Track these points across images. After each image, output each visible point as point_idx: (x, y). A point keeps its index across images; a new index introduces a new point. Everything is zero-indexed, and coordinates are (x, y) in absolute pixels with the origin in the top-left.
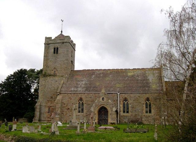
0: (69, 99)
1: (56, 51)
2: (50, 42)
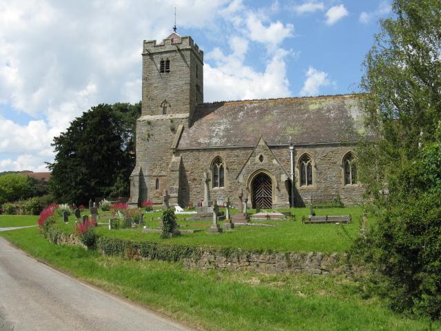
1: (165, 67)
2: (153, 50)
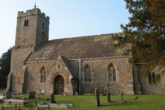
0: (33, 69)
1: (26, 23)
2: (22, 16)
